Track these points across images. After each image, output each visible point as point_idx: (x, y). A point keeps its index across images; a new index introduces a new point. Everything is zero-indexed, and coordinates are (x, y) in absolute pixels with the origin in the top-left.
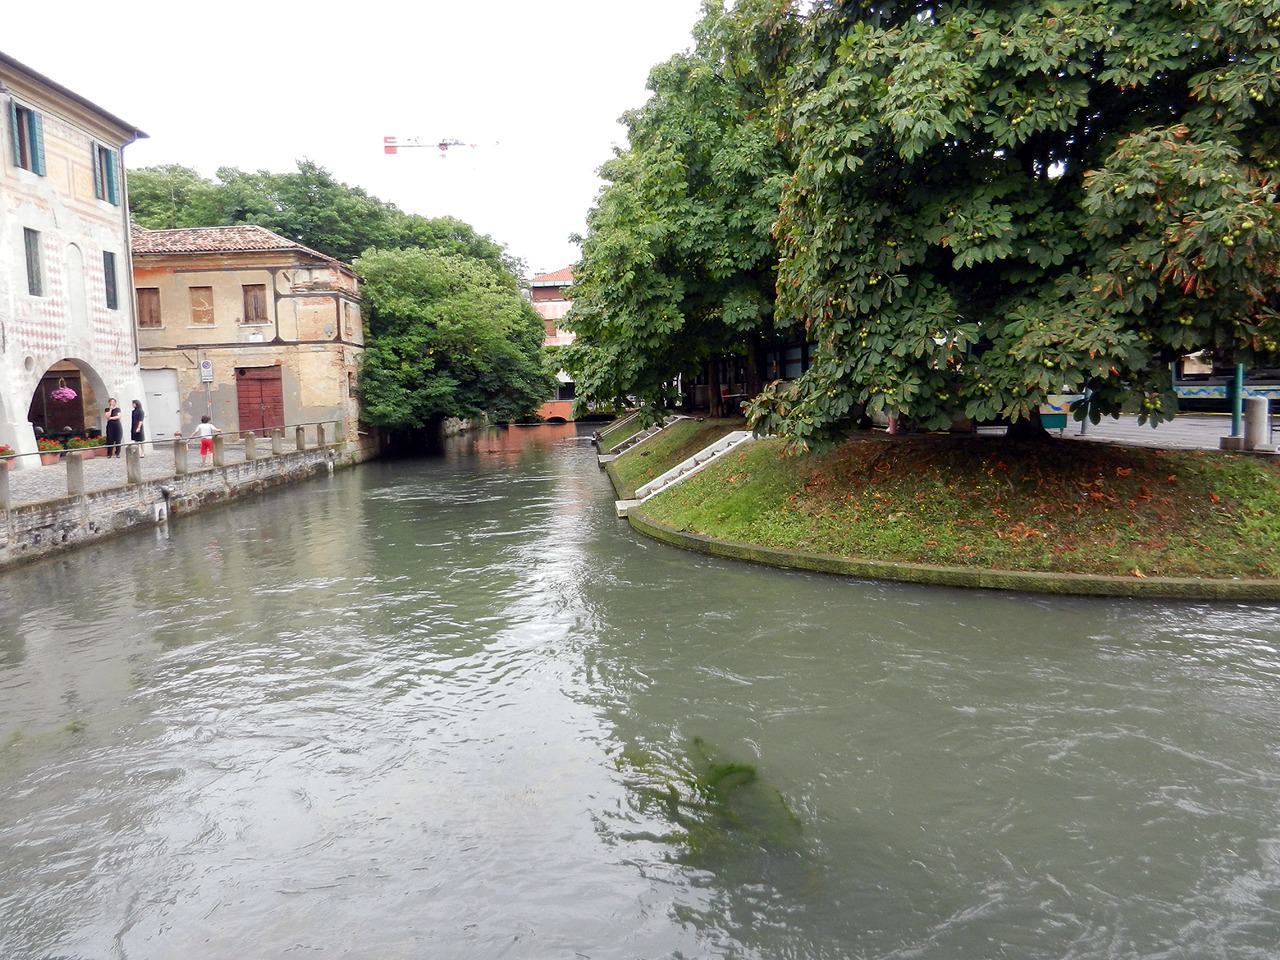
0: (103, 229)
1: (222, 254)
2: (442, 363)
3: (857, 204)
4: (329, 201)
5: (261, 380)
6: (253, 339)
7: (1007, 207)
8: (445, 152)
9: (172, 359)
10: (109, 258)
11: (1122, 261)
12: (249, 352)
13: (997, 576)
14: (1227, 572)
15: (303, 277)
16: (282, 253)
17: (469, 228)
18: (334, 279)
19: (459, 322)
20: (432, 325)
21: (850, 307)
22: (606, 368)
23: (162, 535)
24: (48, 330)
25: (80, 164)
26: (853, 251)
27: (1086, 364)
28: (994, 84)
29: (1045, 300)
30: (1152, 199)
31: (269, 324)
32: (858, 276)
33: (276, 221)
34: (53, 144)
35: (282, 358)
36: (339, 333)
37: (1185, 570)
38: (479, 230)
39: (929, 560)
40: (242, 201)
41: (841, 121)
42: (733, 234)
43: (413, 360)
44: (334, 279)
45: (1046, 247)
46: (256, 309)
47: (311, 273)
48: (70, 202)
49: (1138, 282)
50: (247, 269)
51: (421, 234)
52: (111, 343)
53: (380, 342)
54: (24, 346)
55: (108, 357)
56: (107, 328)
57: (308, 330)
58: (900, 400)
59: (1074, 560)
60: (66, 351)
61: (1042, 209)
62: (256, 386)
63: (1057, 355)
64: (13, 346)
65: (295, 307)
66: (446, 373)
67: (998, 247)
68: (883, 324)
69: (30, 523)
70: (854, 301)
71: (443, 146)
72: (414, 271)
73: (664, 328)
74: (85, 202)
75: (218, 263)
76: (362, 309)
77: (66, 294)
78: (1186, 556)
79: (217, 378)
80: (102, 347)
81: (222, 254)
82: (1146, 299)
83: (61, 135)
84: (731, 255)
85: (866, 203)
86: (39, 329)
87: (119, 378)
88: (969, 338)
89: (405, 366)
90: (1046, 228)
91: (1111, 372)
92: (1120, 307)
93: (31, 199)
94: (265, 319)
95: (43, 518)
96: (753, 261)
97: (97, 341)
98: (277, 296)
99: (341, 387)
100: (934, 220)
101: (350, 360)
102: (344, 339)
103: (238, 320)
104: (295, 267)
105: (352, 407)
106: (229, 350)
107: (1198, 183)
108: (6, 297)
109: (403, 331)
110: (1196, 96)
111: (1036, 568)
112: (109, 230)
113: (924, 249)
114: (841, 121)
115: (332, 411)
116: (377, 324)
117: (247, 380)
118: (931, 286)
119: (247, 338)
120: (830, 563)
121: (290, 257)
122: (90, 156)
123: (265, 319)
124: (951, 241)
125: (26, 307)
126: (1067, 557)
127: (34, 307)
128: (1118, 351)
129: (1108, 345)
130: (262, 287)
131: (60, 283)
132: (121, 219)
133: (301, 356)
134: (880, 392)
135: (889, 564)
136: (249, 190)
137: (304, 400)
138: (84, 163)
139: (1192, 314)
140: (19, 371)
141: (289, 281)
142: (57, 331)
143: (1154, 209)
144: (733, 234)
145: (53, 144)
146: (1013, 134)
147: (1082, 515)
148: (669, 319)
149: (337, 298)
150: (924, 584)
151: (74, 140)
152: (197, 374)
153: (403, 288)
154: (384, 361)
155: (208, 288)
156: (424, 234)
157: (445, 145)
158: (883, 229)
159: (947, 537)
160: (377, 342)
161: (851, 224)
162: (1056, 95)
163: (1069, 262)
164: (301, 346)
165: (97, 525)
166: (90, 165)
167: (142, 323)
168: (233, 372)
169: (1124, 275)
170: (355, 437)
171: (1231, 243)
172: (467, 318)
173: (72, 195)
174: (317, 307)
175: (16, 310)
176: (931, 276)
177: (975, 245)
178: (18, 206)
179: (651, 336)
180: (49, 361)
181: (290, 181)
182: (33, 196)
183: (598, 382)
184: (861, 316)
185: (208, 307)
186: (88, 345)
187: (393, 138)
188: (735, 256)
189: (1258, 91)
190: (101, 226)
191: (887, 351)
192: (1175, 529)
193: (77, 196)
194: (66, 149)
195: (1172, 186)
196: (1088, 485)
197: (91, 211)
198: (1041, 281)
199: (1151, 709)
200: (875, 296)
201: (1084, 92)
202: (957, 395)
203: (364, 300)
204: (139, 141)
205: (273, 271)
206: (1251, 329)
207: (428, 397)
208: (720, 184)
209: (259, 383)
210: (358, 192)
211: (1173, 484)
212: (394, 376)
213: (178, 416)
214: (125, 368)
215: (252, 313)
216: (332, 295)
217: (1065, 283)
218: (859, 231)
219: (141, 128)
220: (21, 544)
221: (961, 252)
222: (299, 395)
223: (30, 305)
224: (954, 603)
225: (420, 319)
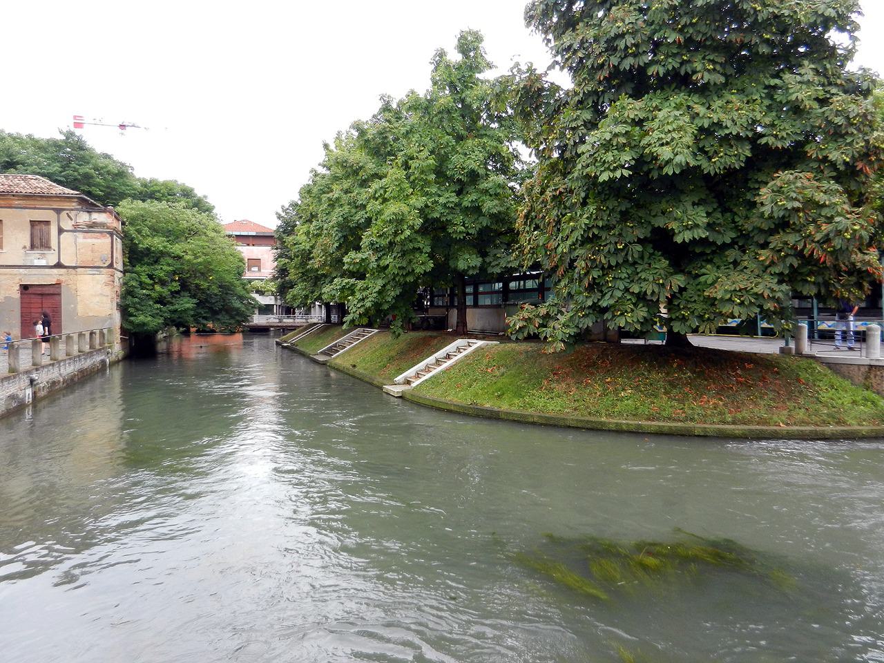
1: (13, 196)
2: (184, 286)
3: (608, 199)
4: (84, 160)
5: (42, 295)
6: (37, 263)
7: (701, 208)
8: (123, 131)
11: (777, 244)
13: (705, 428)
14: (824, 423)
15: (84, 218)
16: (69, 198)
17: (192, 190)
19: (200, 257)
20: (178, 258)
21: (603, 261)
22: (375, 295)
23: (28, 414)
26: (607, 228)
27: (761, 301)
28: (702, 137)
29: (718, 264)
30: (797, 210)
32: (611, 243)
33: (44, 173)
35: (62, 278)
36: (112, 261)
37: (803, 422)
38: (199, 192)
39: (658, 419)
40: (10, 156)
41: (615, 149)
42: (466, 211)
43: (163, 283)
45: (719, 232)
47: (90, 215)
49: (787, 255)
50: (35, 208)
51: (156, 191)
53: (138, 268)
57: (87, 258)
58: (635, 320)
59: (743, 417)
61: (715, 210)
62: (38, 299)
63: (743, 296)
65: (76, 239)
66: (187, 294)
67: (700, 231)
68: (624, 273)
70: (605, 257)
71: (122, 126)
72: (164, 218)
73: (419, 270)
75: (11, 202)
76: (124, 244)
78: (801, 414)
81: (13, 196)
82: (791, 266)
84: (463, 225)
85: (614, 199)
88: (679, 283)
89: (158, 288)
90: (718, 222)
91: (775, 307)
92: (777, 270)
94: (49, 248)
96: (477, 229)
98: (61, 231)
99: (112, 302)
100: (657, 212)
101: (117, 283)
102: (115, 266)
103: (25, 247)
104: (77, 210)
105: (117, 316)
106: (15, 271)
107: (825, 203)
109: (156, 262)
110: (811, 155)
111: (725, 423)
113: (650, 229)
114: (615, 149)
115: (104, 320)
116: (135, 255)
117: (30, 294)
118: (651, 251)
119: (31, 261)
120: (595, 422)
121: (74, 202)
123: (49, 248)
124: (673, 225)
126: (739, 416)
128: (779, 295)
129: (772, 290)
130: (47, 223)
134: (622, 314)
135: (636, 422)
136: (17, 148)
137: (80, 309)
139: (815, 276)
141: (71, 219)
143: (798, 215)
144: (466, 211)
146: (712, 167)
147: (737, 391)
148: (422, 263)
149: (111, 235)
150: (659, 434)
153: (155, 231)
154: (141, 283)
156: (159, 191)
157: (124, 126)
158: (625, 216)
159: (648, 406)
160: (135, 269)
161: (604, 211)
162: (734, 147)
163: (734, 242)
164: (79, 270)
168: (18, 288)
169: (780, 251)
170: (119, 341)
171: (849, 237)
172: (206, 255)
176: (651, 245)
177: (688, 229)
179: (408, 274)
181: (56, 145)
183: (368, 304)
184: (610, 267)
187: (81, 117)
188: (466, 225)
189: (847, 157)
191: (627, 290)
192: (788, 399)
195: (811, 203)
196: (734, 374)
198: (713, 252)
200: (619, 255)
201: (747, 148)
203: (125, 237)
205: (58, 211)
206: (837, 285)
207: (175, 311)
209: (40, 297)
210: (107, 156)
211: (778, 373)
212: (150, 295)
215: (37, 242)
216: (108, 233)
217: (732, 254)
218: (609, 215)
221: (680, 232)
224: (653, 445)
225: (169, 254)
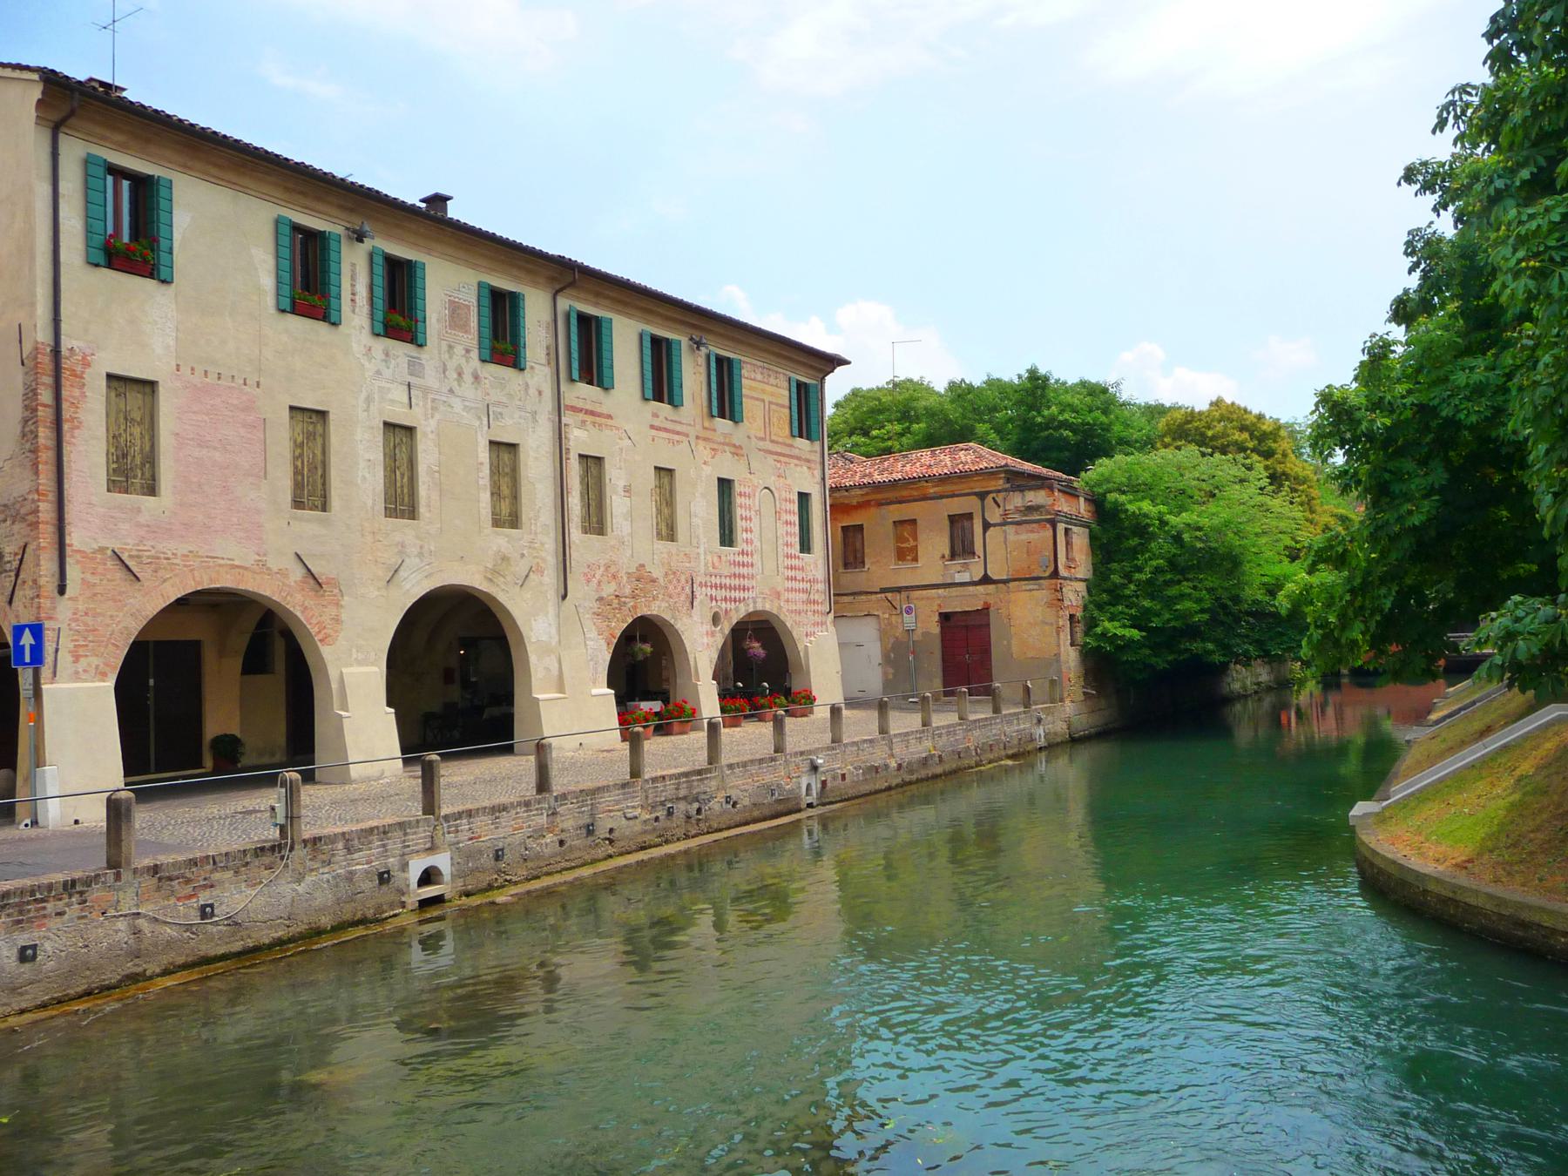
0: (799, 469)
6: (959, 578)
9: (875, 603)
10: (804, 498)
12: (954, 594)
18: (1050, 501)
24: (736, 582)
25: (777, 405)
31: (977, 560)
34: (751, 388)
44: (1050, 501)
46: (963, 542)
48: (767, 445)
52: (805, 591)
54: (712, 600)
55: (800, 607)
56: (799, 575)
60: (755, 603)
64: (701, 602)
65: (1005, 537)
69: (664, 794)
74: (781, 443)
77: (757, 543)
79: (919, 625)
80: (792, 596)
83: (759, 377)
86: (728, 581)
87: (810, 629)
93: (727, 448)
95: (677, 789)
97: (788, 590)
98: (986, 526)
102: (1063, 572)
103: (943, 557)
104: (1006, 490)
108: (697, 550)
112: (805, 468)
119: (953, 576)
122: (787, 393)
125: (716, 559)
127: (723, 558)
130: (970, 516)
131: (751, 531)
132: (818, 455)
133: (1013, 596)
137: (1015, 649)
138: (780, 401)
140: (708, 627)
141: (999, 506)
142: (746, 583)
145: (751, 388)
151: (772, 380)
152: (900, 621)
155: (913, 522)
165: (734, 799)
166: (787, 403)
167: (846, 565)
173: (768, 437)
174: (1033, 536)
175: (706, 565)
178: (713, 457)
180: (739, 613)
182: (728, 445)
185: (912, 543)
186: (778, 595)
190: (796, 465)
193: (773, 438)
194: (763, 391)
197: (786, 451)
199: (1530, 1130)
202: (1446, 660)
204: (839, 370)
205: (982, 496)
208: (356, 581)
213: (880, 669)
214: (818, 618)
215: (959, 548)
216: (1048, 521)
219: (847, 358)
220: (654, 815)
222: (1009, 644)
223: (720, 557)
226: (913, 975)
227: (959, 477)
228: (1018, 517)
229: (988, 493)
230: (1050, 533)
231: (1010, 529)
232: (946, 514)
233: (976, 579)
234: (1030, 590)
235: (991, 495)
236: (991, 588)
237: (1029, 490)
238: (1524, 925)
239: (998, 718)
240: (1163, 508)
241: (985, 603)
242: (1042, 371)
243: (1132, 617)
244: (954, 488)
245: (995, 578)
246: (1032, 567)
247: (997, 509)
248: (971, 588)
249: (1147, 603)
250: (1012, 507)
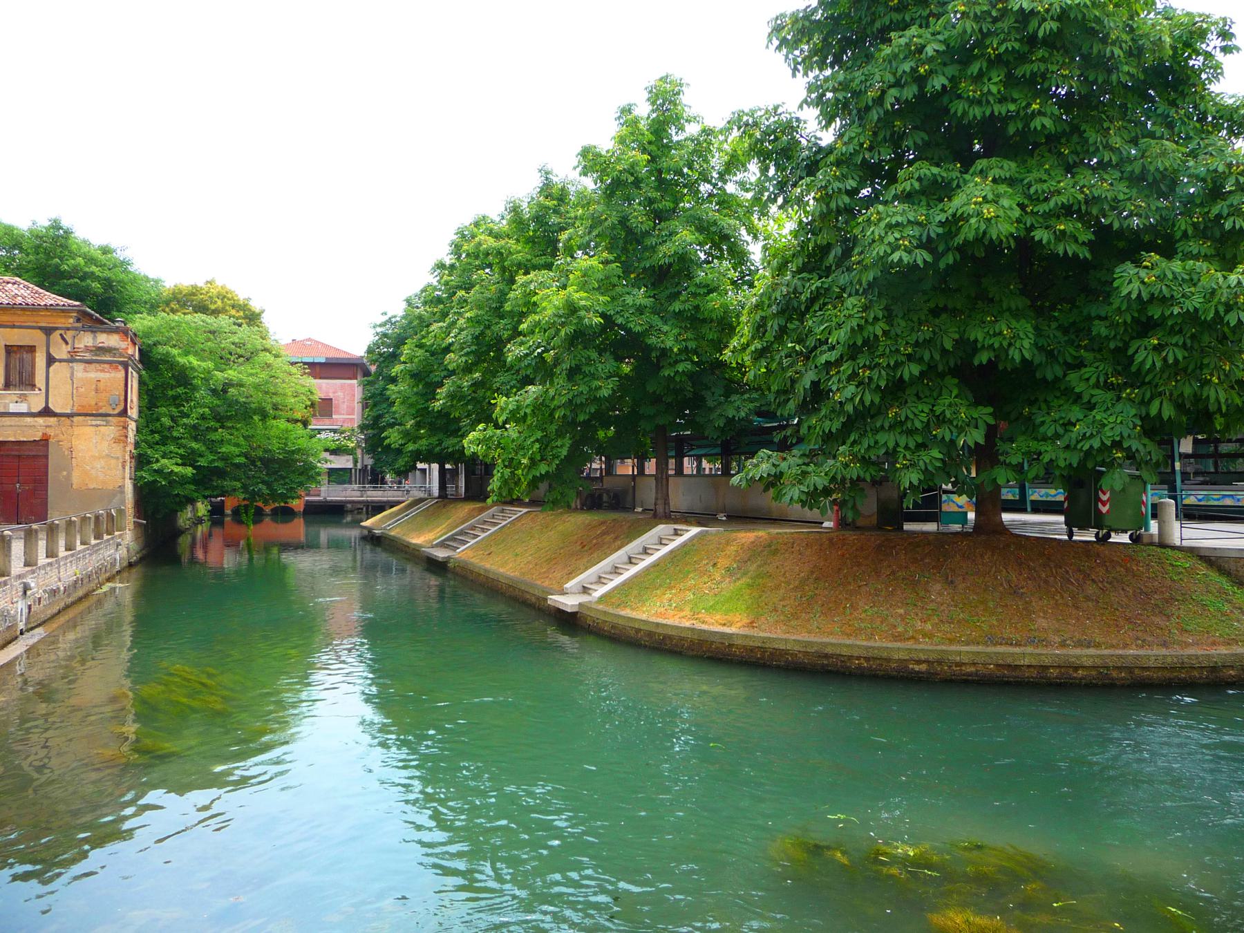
6: (13, 408)
46: (20, 373)
65: (72, 374)
98: (51, 361)
104: (76, 329)
119: (6, 406)
130: (32, 349)
133: (77, 431)
141: (67, 343)
174: (101, 375)
205: (48, 331)
215: (15, 377)
216: (121, 363)
226: (233, 775)
227: (23, 309)
228: (88, 356)
229: (57, 329)
230: (122, 374)
231: (79, 367)
232: (3, 343)
233: (35, 410)
234: (97, 426)
235: (59, 332)
236: (52, 420)
237: (102, 332)
238: (826, 656)
239: (100, 543)
240: (210, 365)
241: (44, 434)
242: (65, 223)
243: (182, 457)
244: (15, 318)
245: (58, 411)
246: (100, 404)
247: (64, 346)
248: (29, 420)
249: (194, 445)
250: (82, 346)
